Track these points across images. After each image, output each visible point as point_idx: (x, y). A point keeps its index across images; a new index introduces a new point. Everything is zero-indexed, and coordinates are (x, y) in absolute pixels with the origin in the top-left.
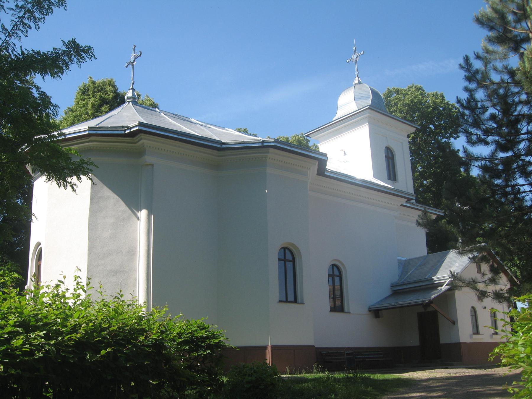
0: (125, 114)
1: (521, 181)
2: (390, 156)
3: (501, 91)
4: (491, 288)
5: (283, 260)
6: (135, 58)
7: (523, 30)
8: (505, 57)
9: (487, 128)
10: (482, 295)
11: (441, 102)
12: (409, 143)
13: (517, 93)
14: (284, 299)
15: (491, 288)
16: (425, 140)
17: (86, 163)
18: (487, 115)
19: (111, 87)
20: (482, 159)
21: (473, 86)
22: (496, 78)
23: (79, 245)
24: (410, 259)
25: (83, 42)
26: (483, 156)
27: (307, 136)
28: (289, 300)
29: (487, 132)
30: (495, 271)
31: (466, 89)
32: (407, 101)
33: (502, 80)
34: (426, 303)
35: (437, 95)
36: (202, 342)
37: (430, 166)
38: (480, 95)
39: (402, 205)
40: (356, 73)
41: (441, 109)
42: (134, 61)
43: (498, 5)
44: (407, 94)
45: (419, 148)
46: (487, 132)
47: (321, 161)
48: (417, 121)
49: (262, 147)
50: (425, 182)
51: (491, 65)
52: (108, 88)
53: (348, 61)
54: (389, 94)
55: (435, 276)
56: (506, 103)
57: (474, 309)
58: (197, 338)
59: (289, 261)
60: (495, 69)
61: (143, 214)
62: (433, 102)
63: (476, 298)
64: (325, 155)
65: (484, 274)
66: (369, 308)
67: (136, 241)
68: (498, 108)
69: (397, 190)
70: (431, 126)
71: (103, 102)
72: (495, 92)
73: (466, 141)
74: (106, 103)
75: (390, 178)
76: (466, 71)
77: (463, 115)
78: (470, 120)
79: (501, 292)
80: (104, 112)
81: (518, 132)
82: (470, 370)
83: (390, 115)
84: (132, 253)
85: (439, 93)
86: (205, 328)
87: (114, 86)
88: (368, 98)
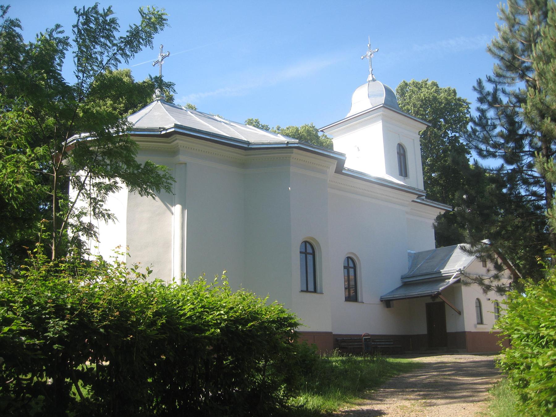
0: (156, 113)
4: (495, 283)
5: (304, 253)
6: (163, 58)
10: (487, 288)
14: (305, 289)
15: (495, 283)
21: (485, 107)
23: (131, 241)
24: (419, 253)
28: (309, 290)
30: (499, 268)
36: (285, 322)
37: (438, 158)
40: (370, 70)
45: (430, 142)
46: (496, 146)
50: (433, 175)
57: (478, 301)
59: (351, 268)
61: (177, 209)
62: (446, 99)
63: (482, 291)
65: (488, 270)
66: (381, 298)
69: (409, 187)
70: (442, 120)
75: (401, 174)
76: (478, 93)
79: (503, 286)
82: (474, 356)
84: (167, 245)
87: (130, 76)
88: (381, 95)
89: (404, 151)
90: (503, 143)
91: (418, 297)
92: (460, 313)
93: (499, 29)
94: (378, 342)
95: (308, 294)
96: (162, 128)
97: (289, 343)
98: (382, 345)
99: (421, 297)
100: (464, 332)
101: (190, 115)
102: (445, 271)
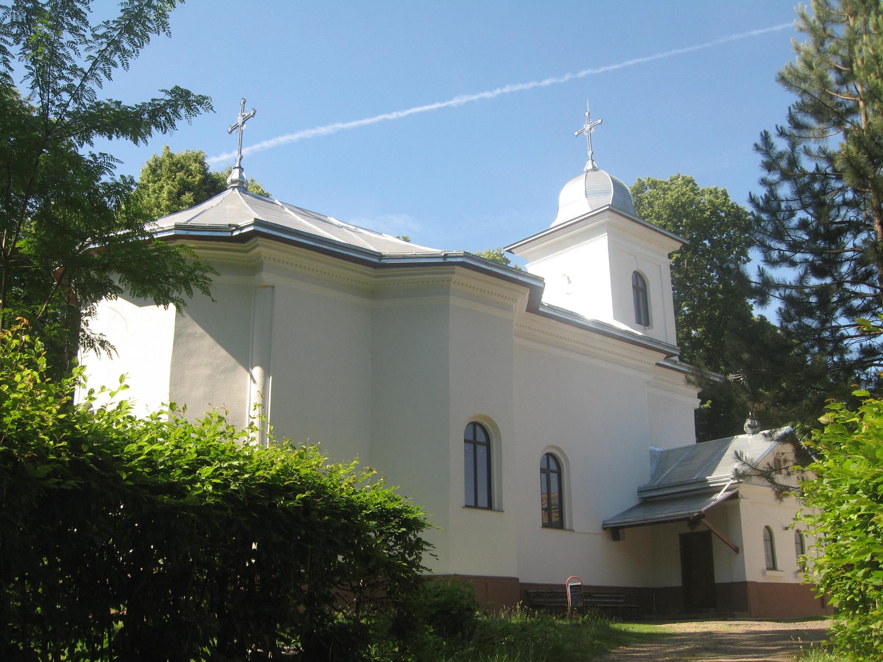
0: (229, 207)
1: (843, 321)
2: (640, 287)
3: (817, 186)
7: (850, 95)
8: (823, 134)
9: (794, 240)
11: (724, 204)
12: (671, 267)
13: (840, 189)
14: (473, 504)
16: (696, 264)
17: (201, 270)
18: (795, 221)
19: (197, 165)
20: (786, 287)
21: (774, 177)
22: (808, 165)
24: (669, 451)
25: (196, 91)
26: (788, 283)
27: (509, 251)
28: (479, 505)
29: (795, 247)
31: (764, 182)
32: (669, 200)
33: (817, 168)
34: (695, 517)
35: (717, 193)
38: (785, 191)
39: (658, 364)
40: (590, 153)
41: (723, 214)
42: (243, 123)
43: (813, 56)
44: (669, 189)
47: (533, 288)
48: (683, 233)
49: (445, 263)
50: (693, 332)
51: (802, 146)
52: (194, 166)
53: (576, 134)
54: (640, 188)
55: (710, 475)
56: (822, 204)
58: (388, 511)
59: (482, 444)
60: (807, 152)
62: (710, 201)
64: (541, 280)
66: (604, 525)
67: (245, 405)
68: (811, 211)
69: (651, 340)
70: (706, 242)
71: (185, 187)
72: (807, 187)
73: (762, 258)
74: (189, 190)
75: (639, 322)
77: (758, 220)
78: (770, 228)
80: (186, 203)
81: (842, 248)
83: (641, 221)
85: (720, 189)
86: (396, 500)
87: (202, 163)
88: (606, 193)
89: (645, 285)
91: (665, 522)
92: (737, 550)
93: (798, 49)
95: (478, 511)
96: (234, 226)
97: (262, 441)
98: (606, 603)
99: (672, 521)
101: (287, 213)
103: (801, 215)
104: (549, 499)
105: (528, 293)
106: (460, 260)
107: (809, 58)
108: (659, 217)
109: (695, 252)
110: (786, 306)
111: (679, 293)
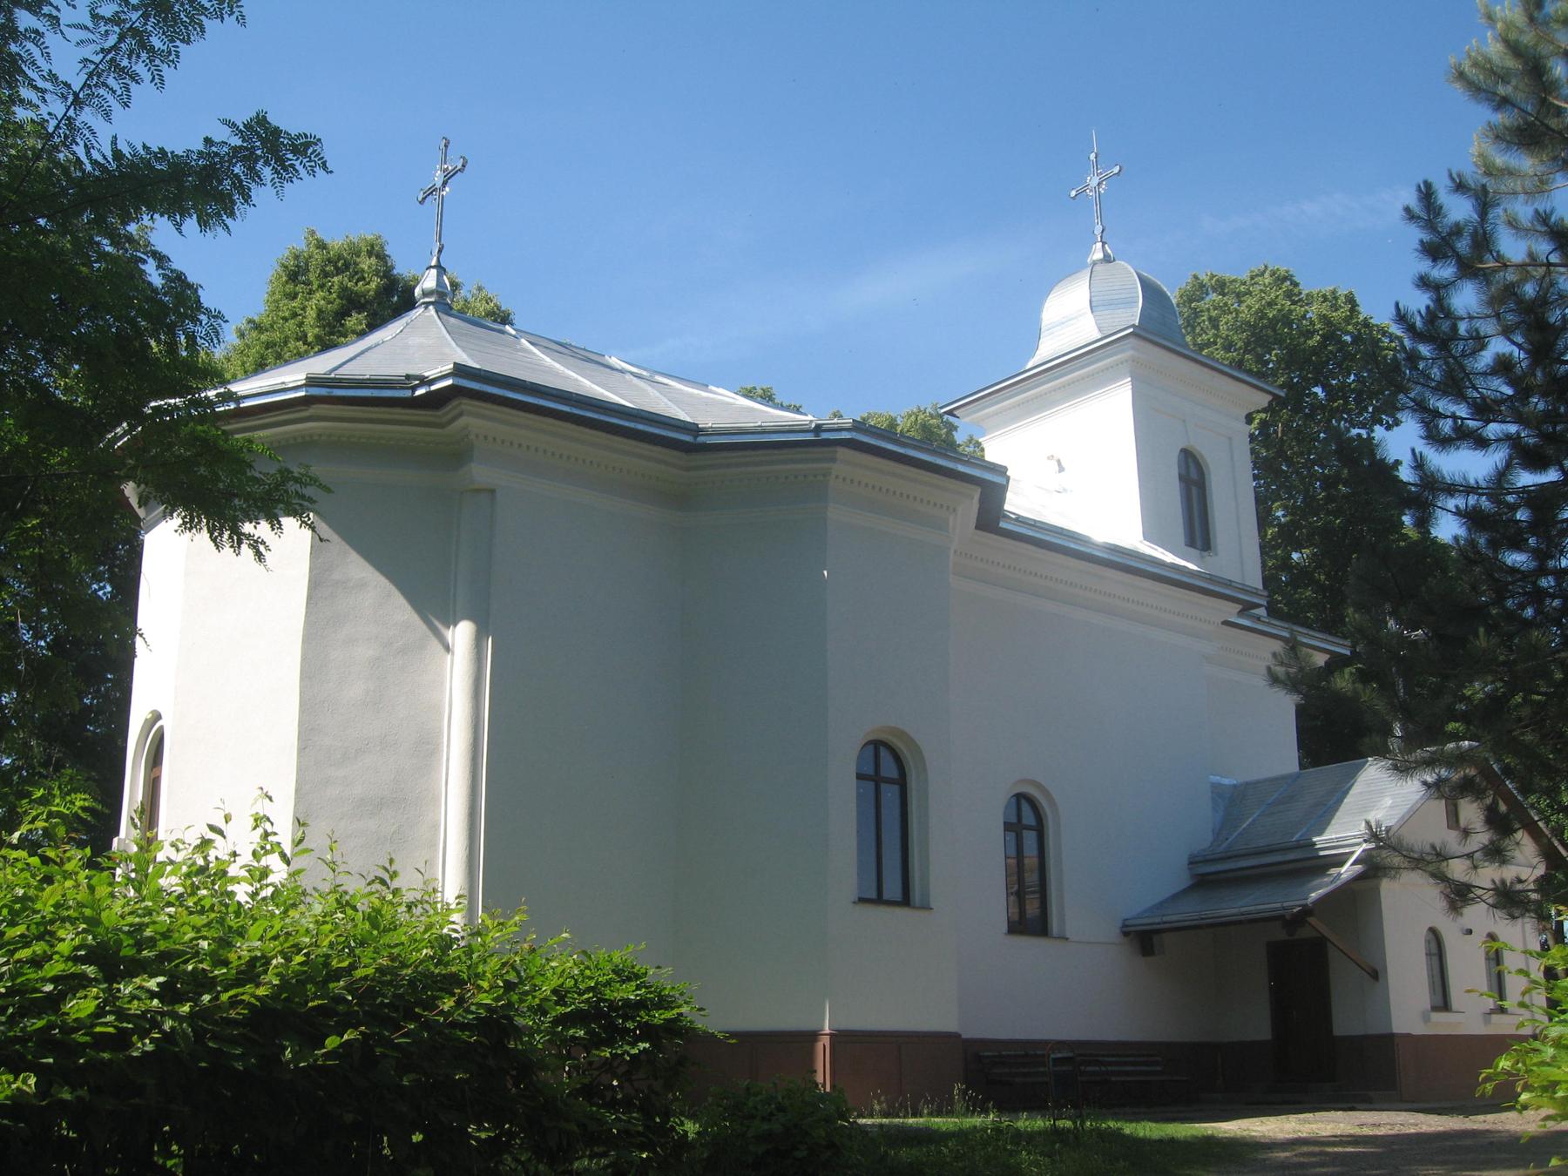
0: (415, 340)
2: (1193, 478)
3: (1529, 290)
4: (1488, 875)
6: (448, 177)
9: (1483, 398)
10: (1459, 895)
11: (1348, 320)
12: (1252, 437)
14: (874, 895)
16: (1298, 431)
18: (1486, 358)
19: (373, 260)
20: (1469, 490)
21: (1445, 272)
23: (272, 722)
24: (1247, 784)
25: (289, 122)
26: (1472, 482)
27: (950, 413)
28: (886, 896)
29: (1486, 410)
31: (1424, 282)
32: (1245, 315)
33: (1531, 255)
35: (1336, 298)
37: (1311, 506)
39: (1226, 623)
40: (1098, 229)
41: (1348, 338)
42: (445, 184)
43: (1522, 32)
44: (1250, 293)
47: (990, 488)
50: (1295, 556)
52: (366, 263)
53: (1073, 193)
54: (1198, 290)
55: (1320, 834)
58: (612, 1005)
59: (890, 781)
60: (1513, 224)
61: (462, 634)
62: (1324, 318)
63: (1442, 904)
64: (1001, 470)
65: (1466, 833)
66: (1124, 926)
68: (1520, 340)
69: (1211, 579)
70: (1318, 390)
71: (352, 302)
73: (1422, 433)
74: (361, 309)
75: (1191, 542)
77: (1413, 357)
78: (1436, 373)
79: (1519, 887)
80: (354, 332)
82: (1421, 1117)
84: (428, 748)
85: (1342, 292)
86: (637, 977)
87: (382, 257)
90: (1510, 397)
91: (1240, 922)
92: (1375, 974)
93: (1490, 18)
94: (1110, 1064)
98: (1127, 1073)
100: (1391, 1037)
102: (1327, 840)
103: (1499, 346)
104: (1021, 880)
105: (977, 496)
106: (845, 435)
107: (1513, 36)
108: (1228, 347)
109: (1297, 409)
110: (1469, 530)
111: (1268, 485)
